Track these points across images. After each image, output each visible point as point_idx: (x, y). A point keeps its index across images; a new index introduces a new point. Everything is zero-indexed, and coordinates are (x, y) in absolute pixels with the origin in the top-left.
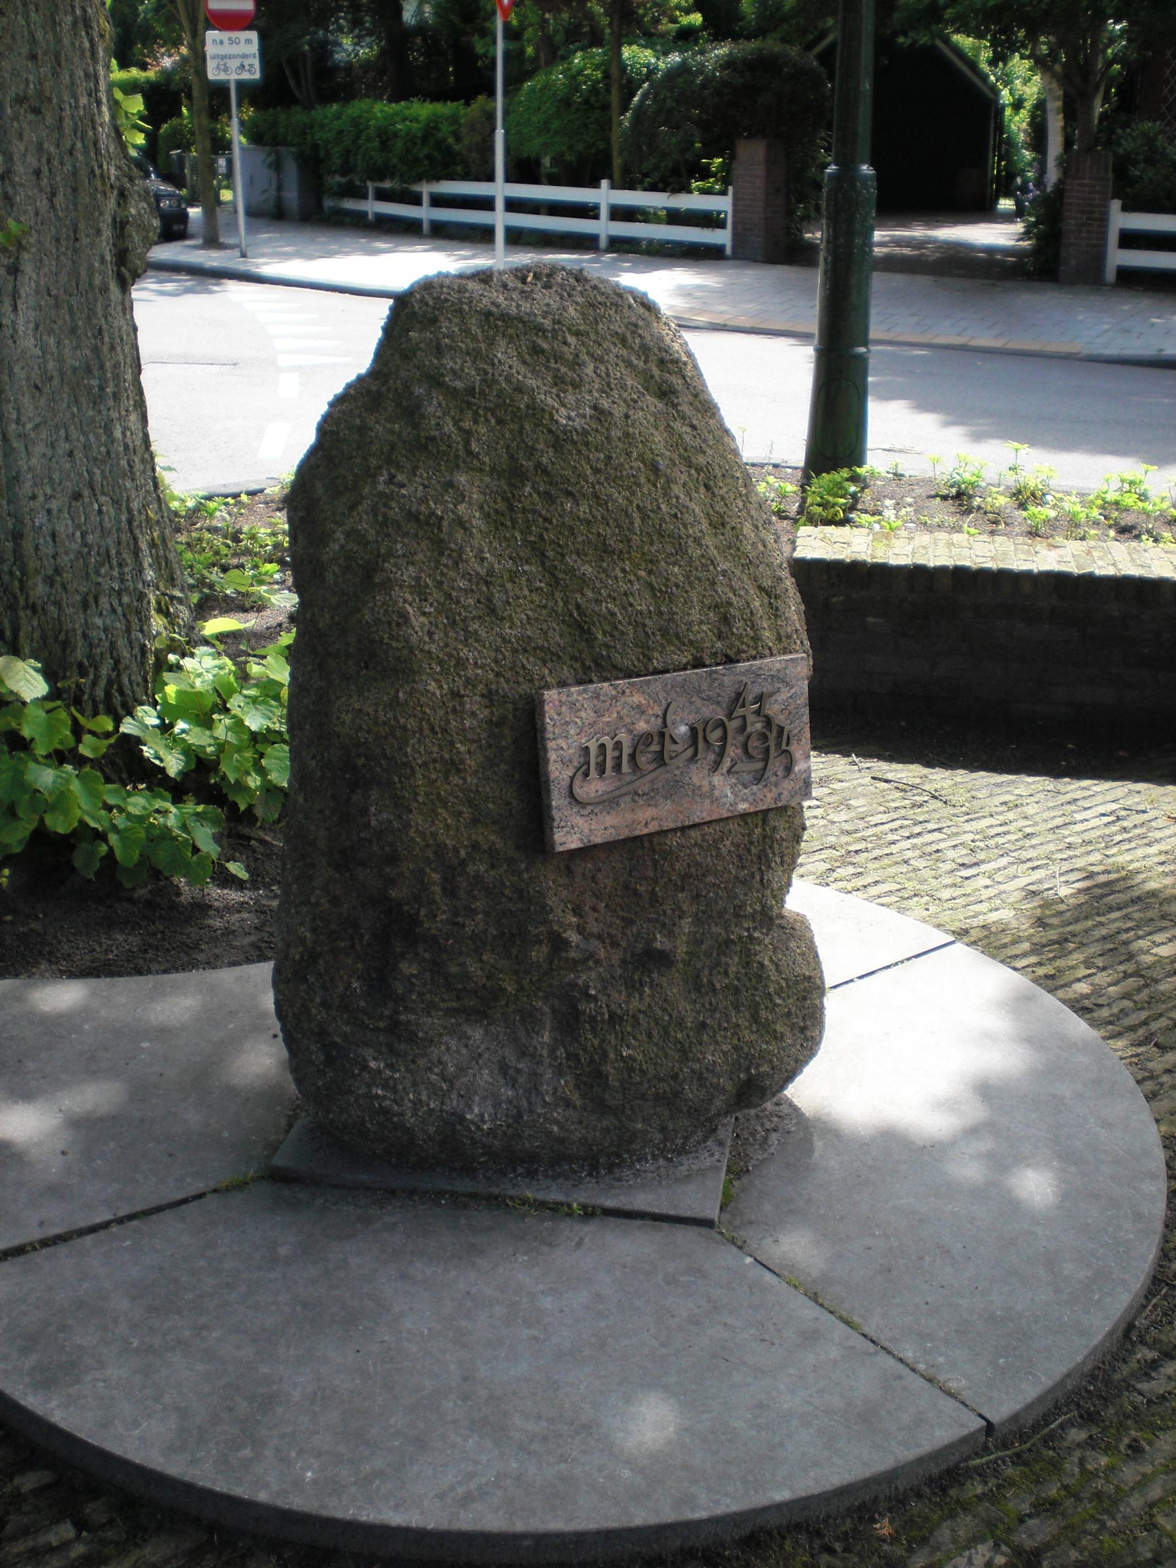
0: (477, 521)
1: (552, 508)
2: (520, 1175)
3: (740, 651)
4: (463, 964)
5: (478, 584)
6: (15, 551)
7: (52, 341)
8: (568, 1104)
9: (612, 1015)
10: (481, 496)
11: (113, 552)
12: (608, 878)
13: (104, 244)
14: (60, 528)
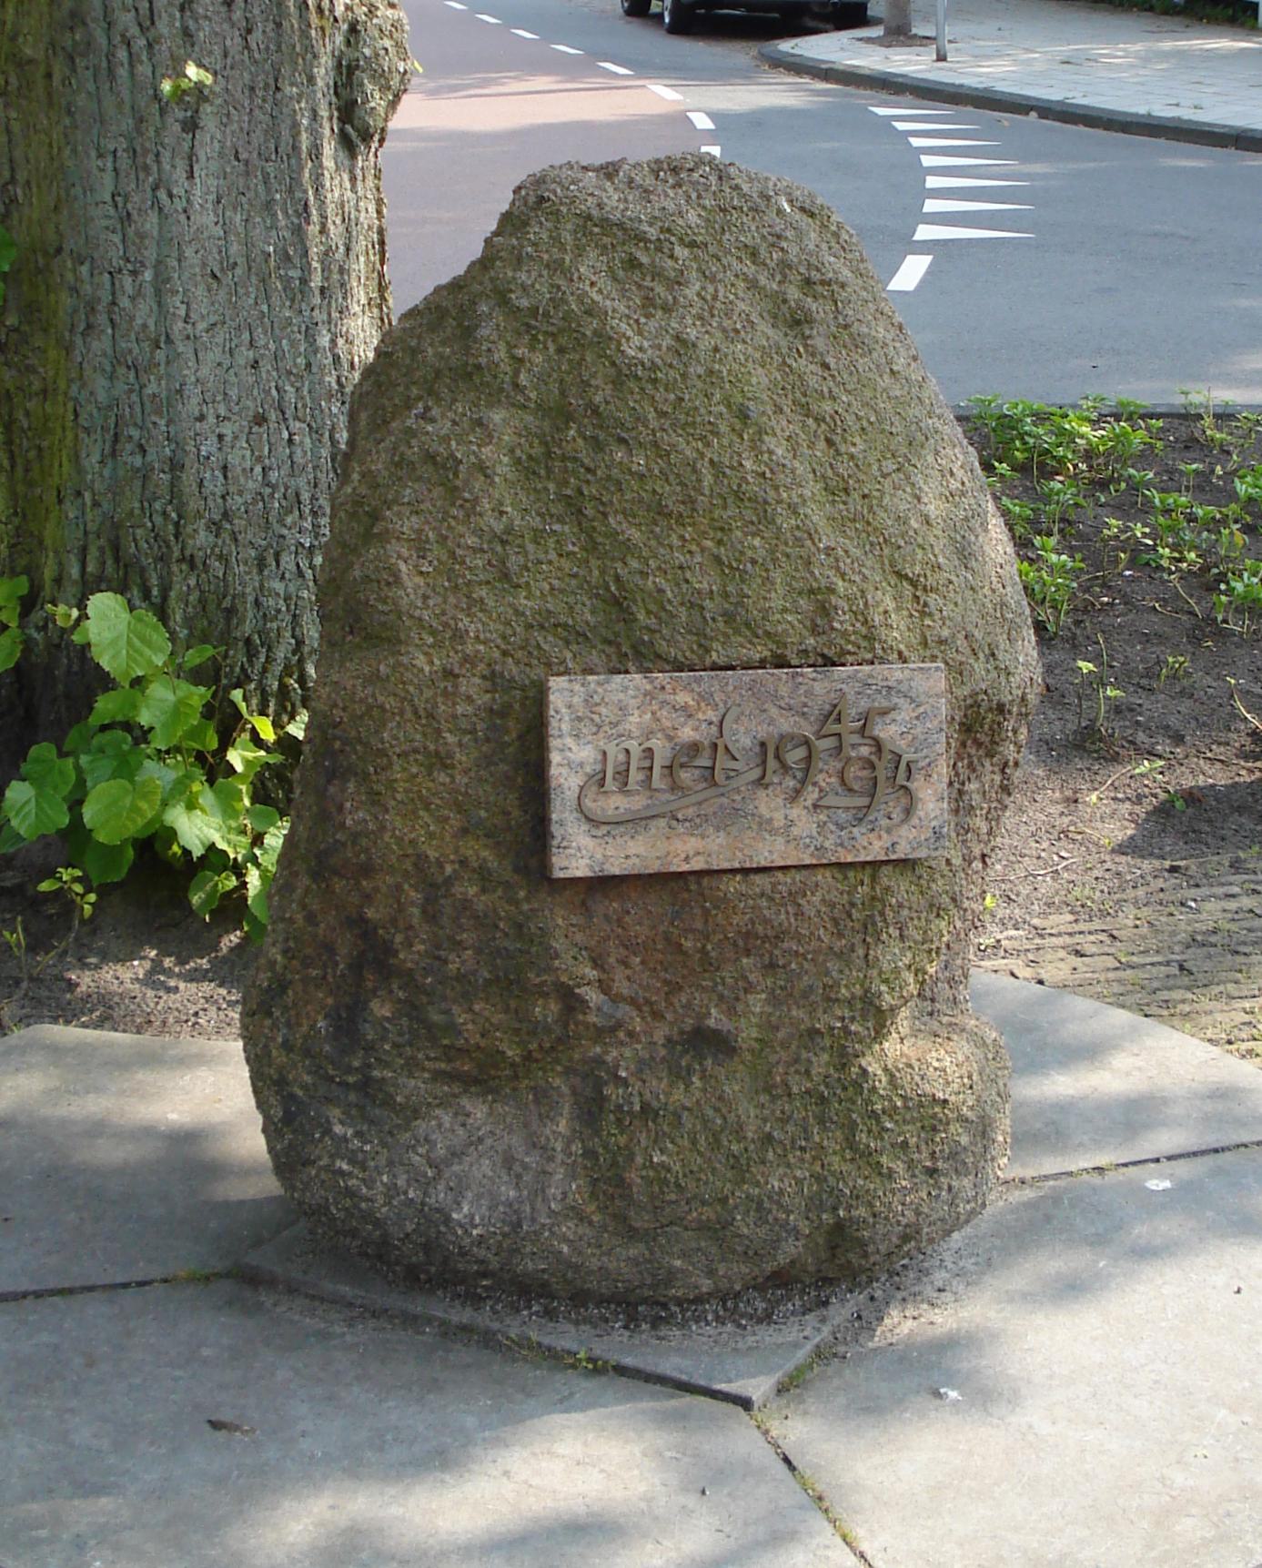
0: (503, 467)
1: (600, 456)
2: (537, 1313)
3: (844, 653)
4: (447, 1012)
5: (490, 542)
6: (172, 485)
7: (238, 218)
8: (582, 1218)
9: (645, 1107)
10: (515, 438)
11: (305, 496)
12: (640, 924)
13: (320, 95)
14: (234, 459)
